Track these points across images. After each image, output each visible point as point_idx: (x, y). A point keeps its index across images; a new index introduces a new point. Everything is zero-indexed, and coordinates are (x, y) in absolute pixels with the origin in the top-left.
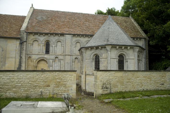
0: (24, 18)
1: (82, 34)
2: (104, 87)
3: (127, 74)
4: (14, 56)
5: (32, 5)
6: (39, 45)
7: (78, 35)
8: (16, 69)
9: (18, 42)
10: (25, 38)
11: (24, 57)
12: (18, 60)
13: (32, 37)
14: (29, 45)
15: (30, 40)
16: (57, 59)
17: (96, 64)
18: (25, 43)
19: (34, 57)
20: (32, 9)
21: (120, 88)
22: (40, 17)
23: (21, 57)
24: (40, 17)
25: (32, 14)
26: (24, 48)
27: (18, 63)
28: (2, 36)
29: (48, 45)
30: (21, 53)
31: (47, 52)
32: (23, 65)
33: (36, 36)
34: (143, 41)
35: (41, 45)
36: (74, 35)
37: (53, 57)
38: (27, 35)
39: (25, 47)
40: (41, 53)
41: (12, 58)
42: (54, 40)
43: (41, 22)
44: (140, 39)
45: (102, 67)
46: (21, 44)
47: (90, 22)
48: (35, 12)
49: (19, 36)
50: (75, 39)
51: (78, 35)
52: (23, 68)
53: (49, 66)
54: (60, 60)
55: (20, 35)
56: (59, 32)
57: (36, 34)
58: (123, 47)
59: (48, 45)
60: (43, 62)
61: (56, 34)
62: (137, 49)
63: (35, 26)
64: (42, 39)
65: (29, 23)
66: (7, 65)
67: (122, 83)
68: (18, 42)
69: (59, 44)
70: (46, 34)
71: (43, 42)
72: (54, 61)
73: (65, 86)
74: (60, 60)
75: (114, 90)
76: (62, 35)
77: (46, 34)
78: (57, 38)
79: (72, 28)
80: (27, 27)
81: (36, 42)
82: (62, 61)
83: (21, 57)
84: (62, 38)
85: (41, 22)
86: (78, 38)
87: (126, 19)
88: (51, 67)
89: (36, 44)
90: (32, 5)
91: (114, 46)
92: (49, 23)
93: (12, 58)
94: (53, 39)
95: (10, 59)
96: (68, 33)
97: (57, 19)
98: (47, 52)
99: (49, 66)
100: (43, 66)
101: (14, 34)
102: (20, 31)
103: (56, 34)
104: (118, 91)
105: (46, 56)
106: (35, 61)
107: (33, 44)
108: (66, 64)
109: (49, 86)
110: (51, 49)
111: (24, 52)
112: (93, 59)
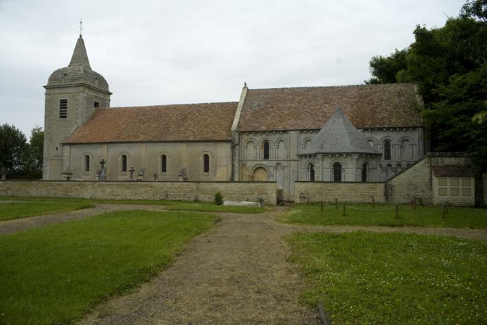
0: (237, 103)
1: (313, 128)
2: (302, 197)
3: (326, 185)
4: (225, 164)
5: (245, 84)
6: (255, 147)
7: (308, 131)
8: (228, 180)
9: (228, 146)
10: (237, 140)
11: (236, 165)
12: (230, 169)
13: (245, 138)
14: (243, 148)
15: (243, 141)
16: (279, 167)
17: (311, 174)
18: (237, 147)
19: (249, 164)
20: (246, 90)
21: (318, 199)
22: (255, 104)
23: (233, 165)
24: (255, 104)
25: (245, 100)
26: (237, 153)
27: (230, 173)
28: (211, 139)
29: (266, 146)
30: (233, 160)
31: (266, 156)
32: (236, 175)
33: (251, 136)
34: (421, 131)
35: (258, 147)
36: (302, 131)
37: (274, 163)
38: (239, 135)
39: (237, 151)
40: (258, 159)
41: (223, 166)
42: (274, 140)
43: (257, 112)
44: (414, 128)
45: (316, 180)
46: (233, 147)
47: (332, 103)
48: (250, 95)
49: (230, 138)
50: (303, 136)
51: (308, 131)
52: (236, 179)
53: (269, 177)
54: (283, 168)
55: (231, 136)
56: (281, 128)
57: (250, 132)
58: (337, 155)
59: (266, 146)
60: (261, 170)
61: (277, 131)
62: (356, 157)
63: (249, 120)
64: (259, 139)
65: (241, 116)
66: (218, 176)
67: (321, 194)
68: (228, 146)
69: (282, 144)
70: (264, 132)
71: (260, 144)
72: (276, 168)
73: (266, 194)
74: (283, 168)
75: (312, 200)
76: (285, 131)
77: (264, 132)
78: (278, 136)
79: (300, 119)
80: (239, 122)
81: (251, 144)
82: (286, 169)
83: (233, 165)
84: (285, 136)
85: (257, 112)
86: (308, 135)
87: (403, 88)
88: (272, 178)
89: (251, 146)
90: (245, 84)
91: (325, 155)
92: (268, 113)
93: (223, 166)
94: (273, 139)
95: (222, 168)
96: (292, 129)
97: (280, 105)
98: (266, 156)
99: (269, 177)
100: (260, 176)
101: (224, 135)
102: (230, 130)
103: (277, 131)
104: (317, 201)
105: (264, 162)
106: (250, 168)
107: (247, 147)
108: (291, 174)
109: (253, 194)
110: (271, 152)
111: (237, 158)
112: (308, 169)
